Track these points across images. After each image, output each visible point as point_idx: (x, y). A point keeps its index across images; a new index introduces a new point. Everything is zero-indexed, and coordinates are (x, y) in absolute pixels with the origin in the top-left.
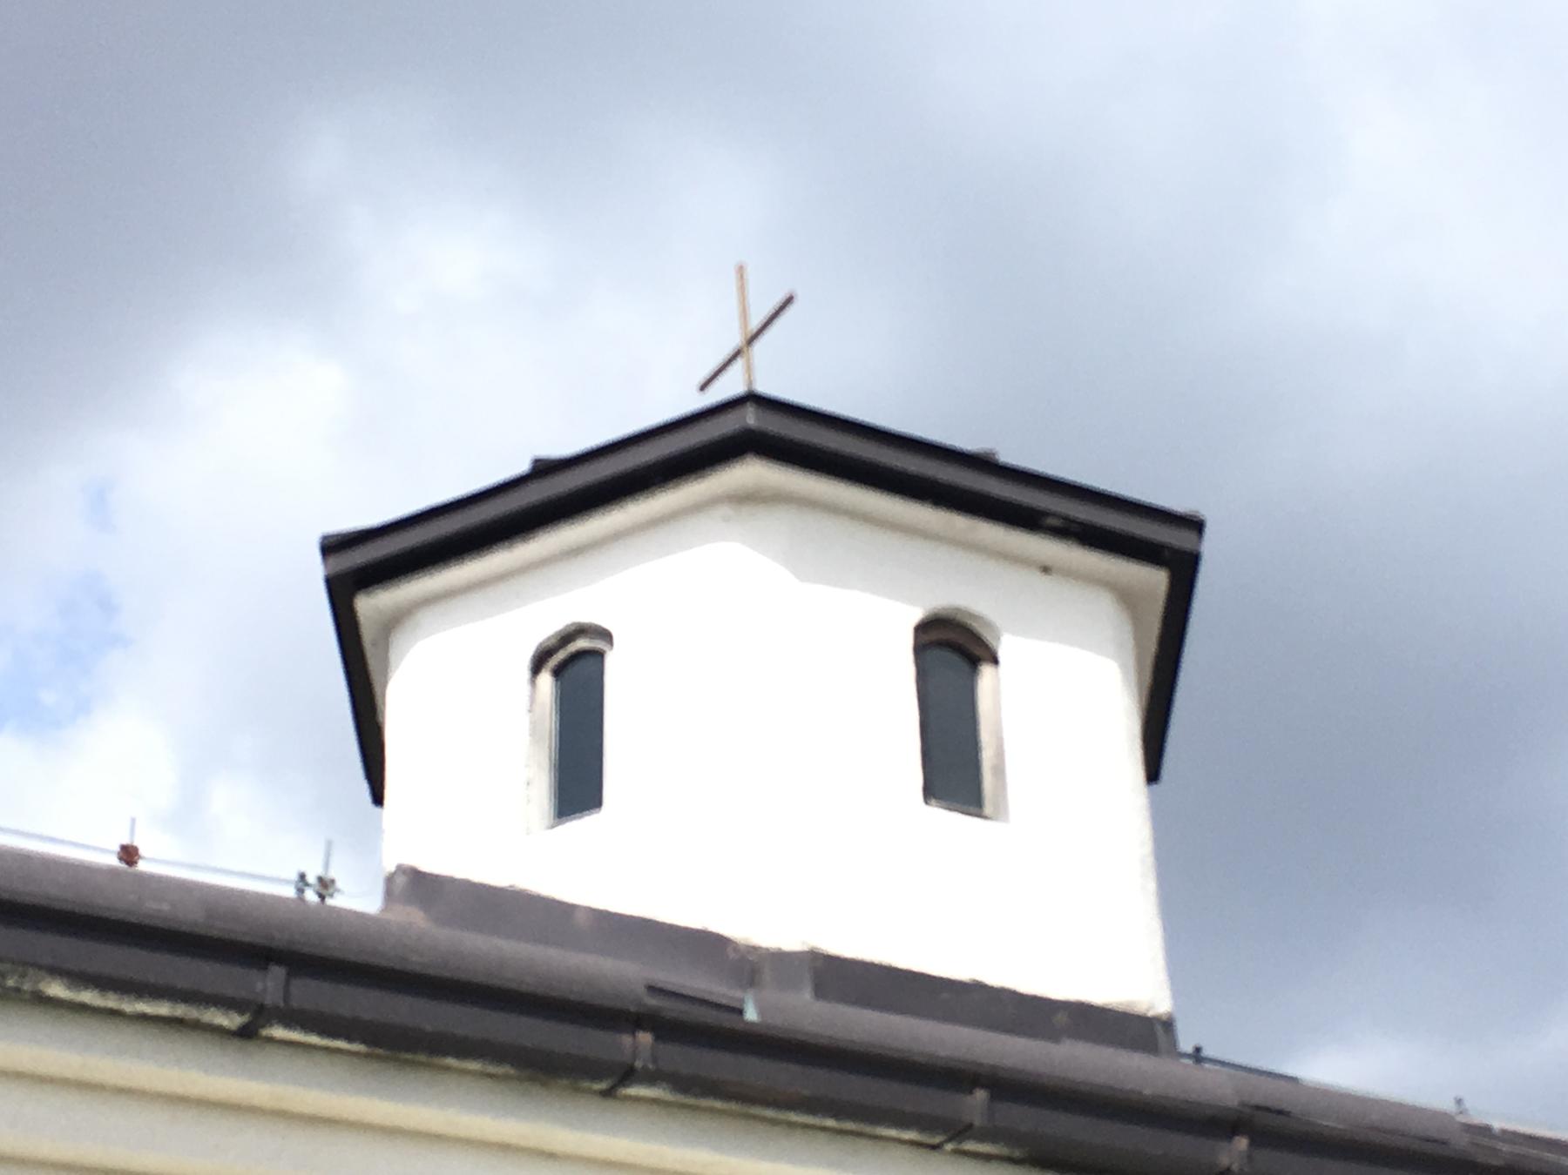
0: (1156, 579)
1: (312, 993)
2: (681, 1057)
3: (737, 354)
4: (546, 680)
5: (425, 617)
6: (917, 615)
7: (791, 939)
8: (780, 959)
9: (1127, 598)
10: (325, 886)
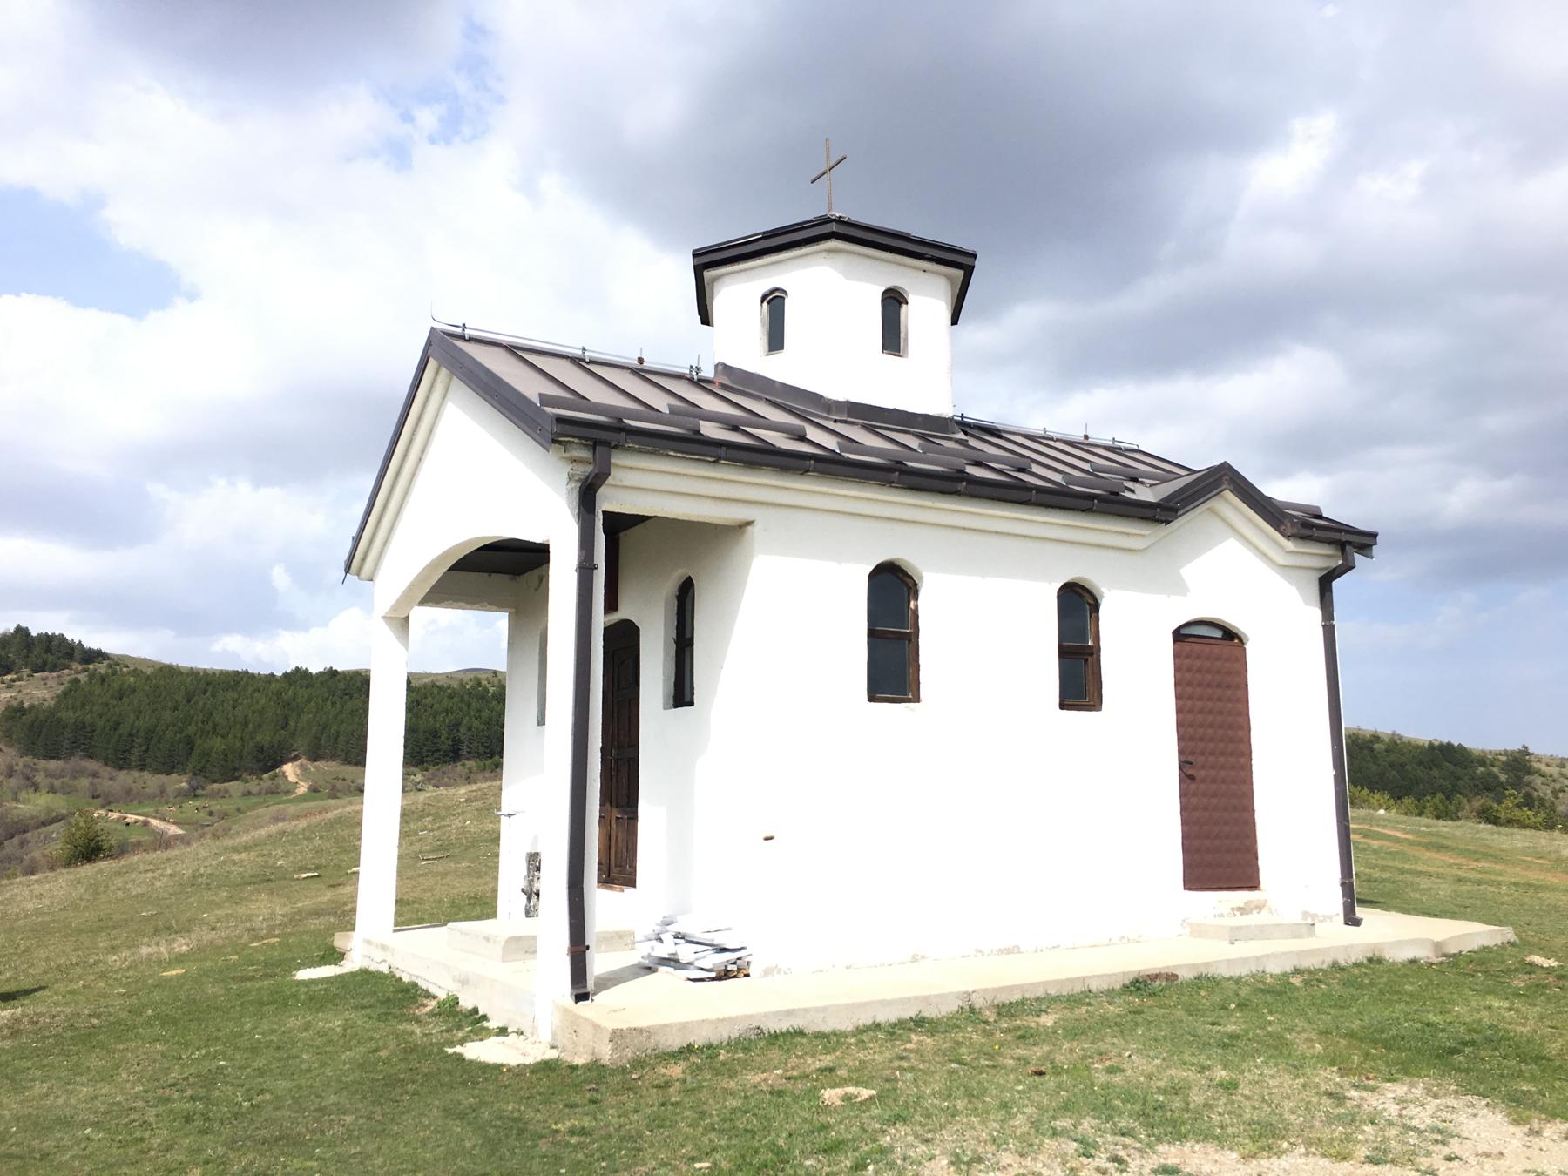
0: (960, 273)
1: (732, 453)
2: (820, 465)
3: (825, 173)
4: (765, 304)
5: (726, 279)
6: (883, 289)
7: (841, 398)
8: (838, 403)
9: (949, 278)
10: (698, 369)
